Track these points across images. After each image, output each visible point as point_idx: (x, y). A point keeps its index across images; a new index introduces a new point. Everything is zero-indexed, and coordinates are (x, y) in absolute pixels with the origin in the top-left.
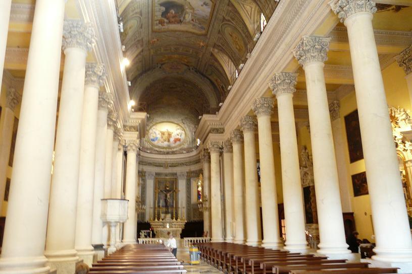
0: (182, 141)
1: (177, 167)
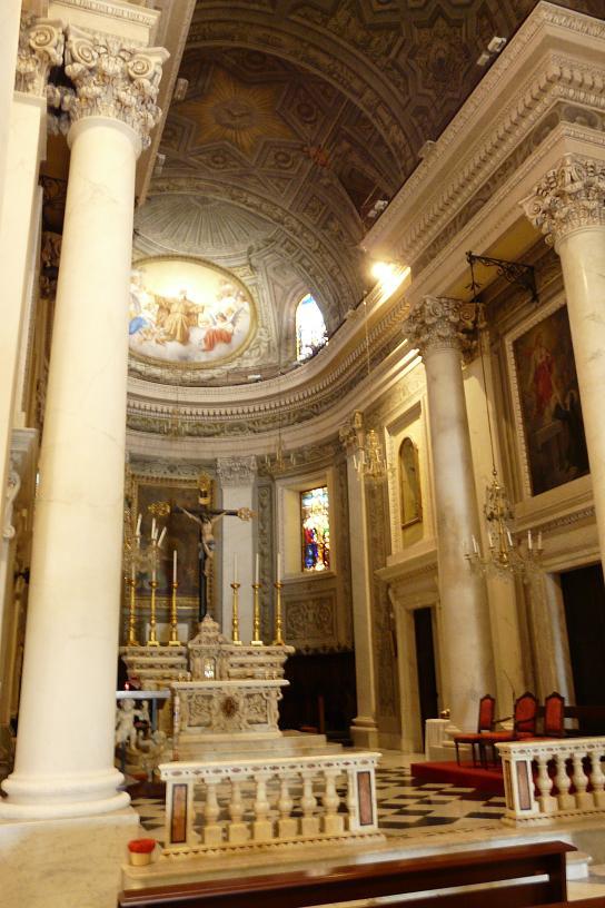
0: (236, 341)
1: (216, 439)
